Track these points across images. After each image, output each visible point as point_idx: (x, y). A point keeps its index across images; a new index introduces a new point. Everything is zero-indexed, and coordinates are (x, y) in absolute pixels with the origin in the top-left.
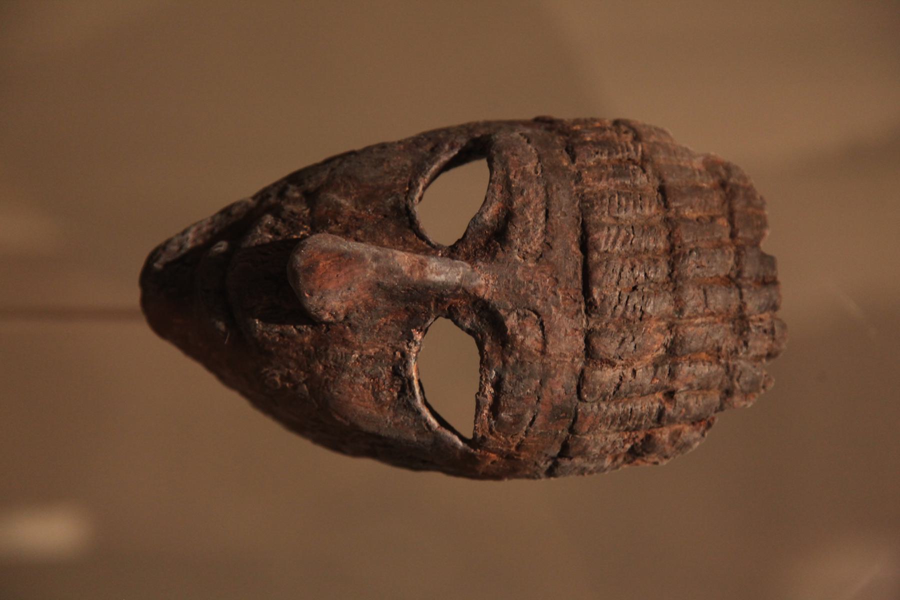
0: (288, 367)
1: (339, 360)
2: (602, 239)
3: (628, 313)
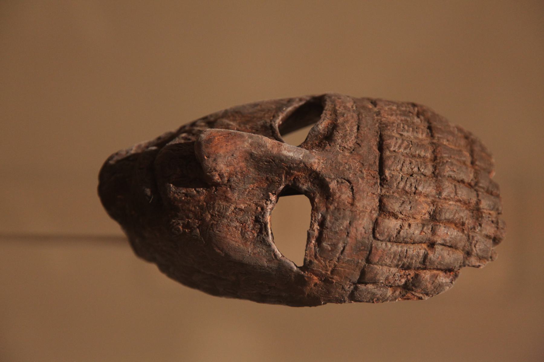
0: (188, 217)
1: (221, 210)
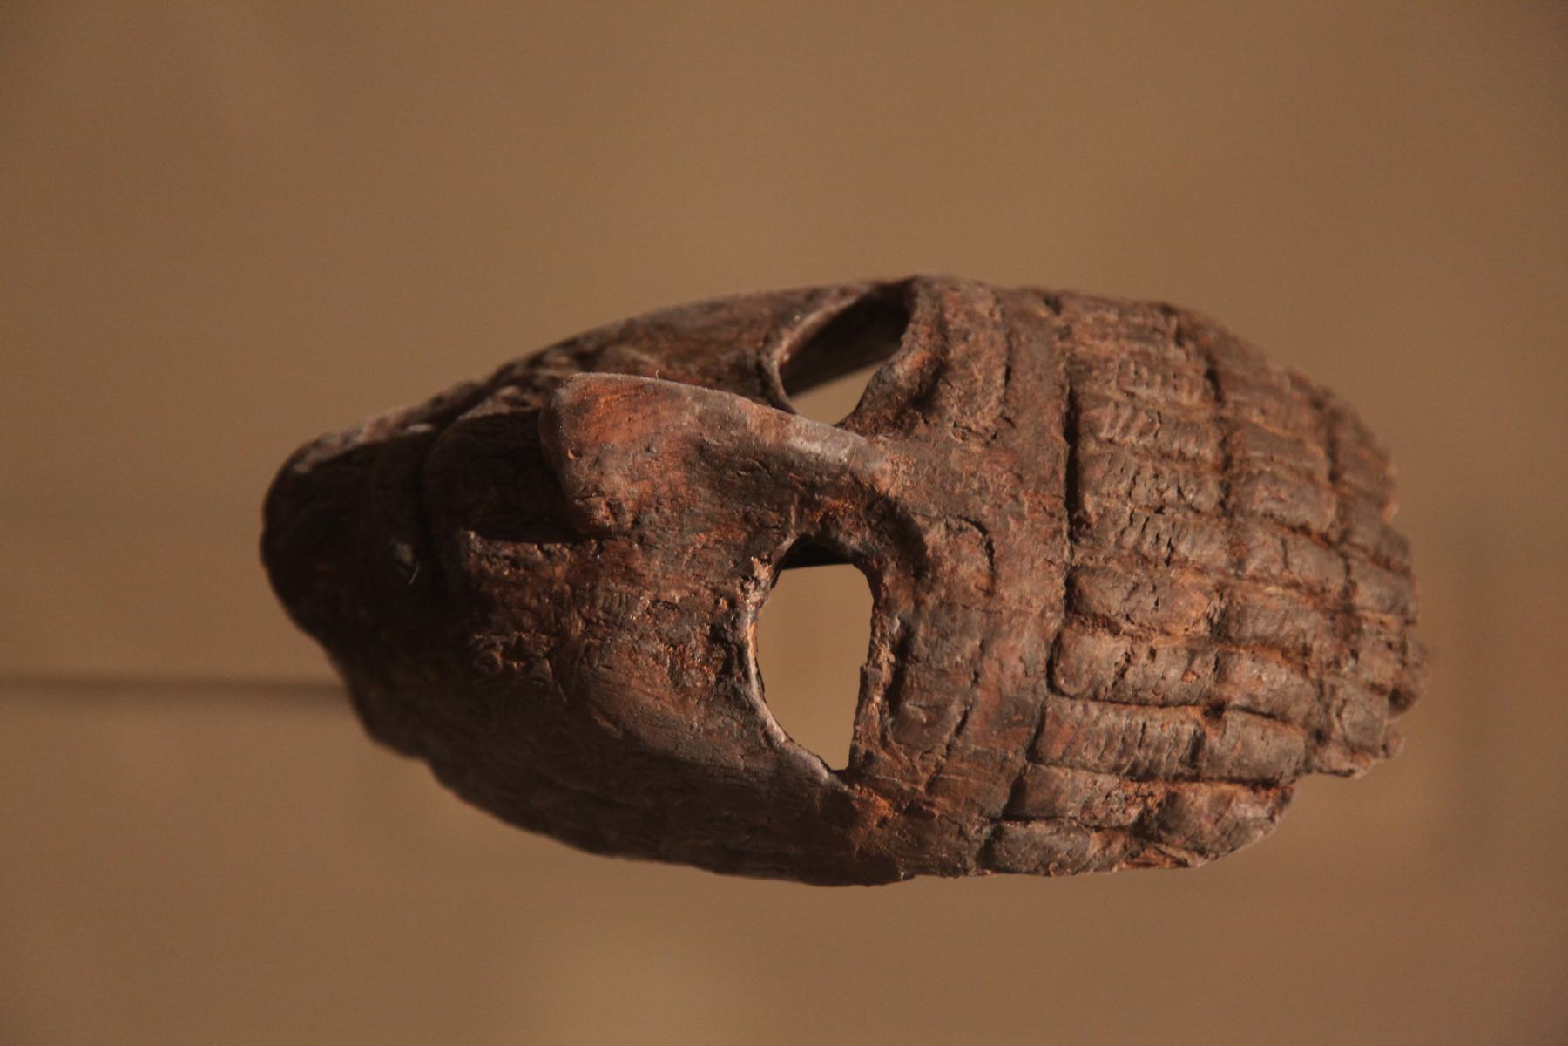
0: (520, 627)
2: (1106, 421)
3: (1146, 547)
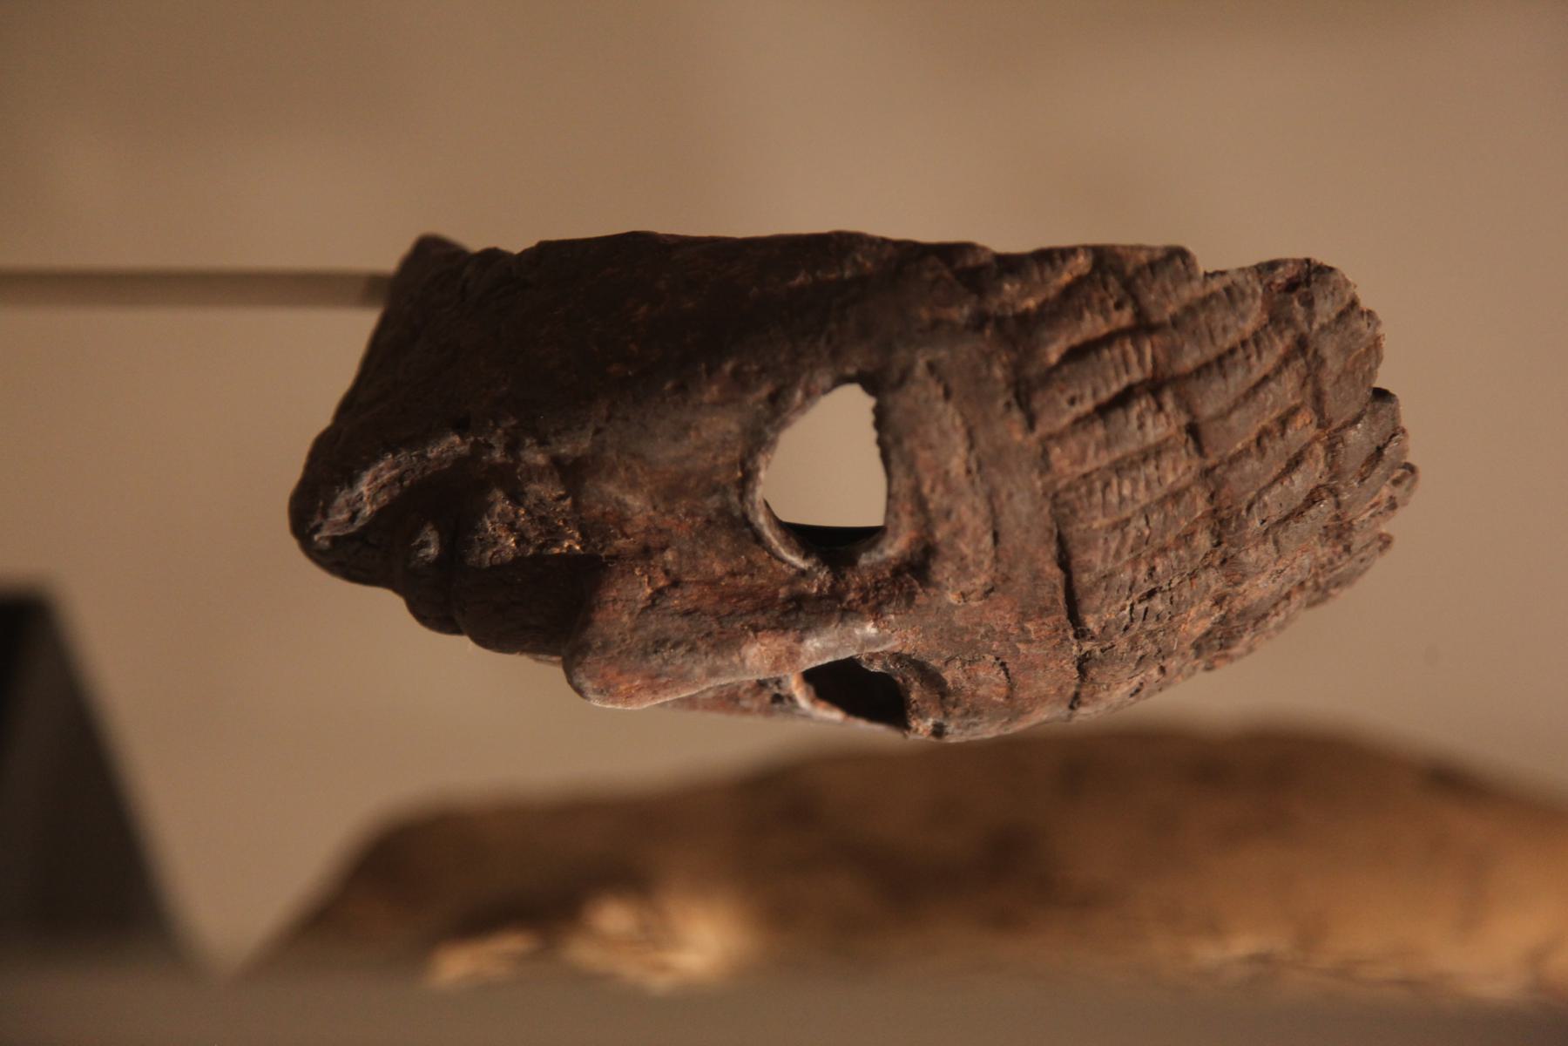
2: (1095, 560)
